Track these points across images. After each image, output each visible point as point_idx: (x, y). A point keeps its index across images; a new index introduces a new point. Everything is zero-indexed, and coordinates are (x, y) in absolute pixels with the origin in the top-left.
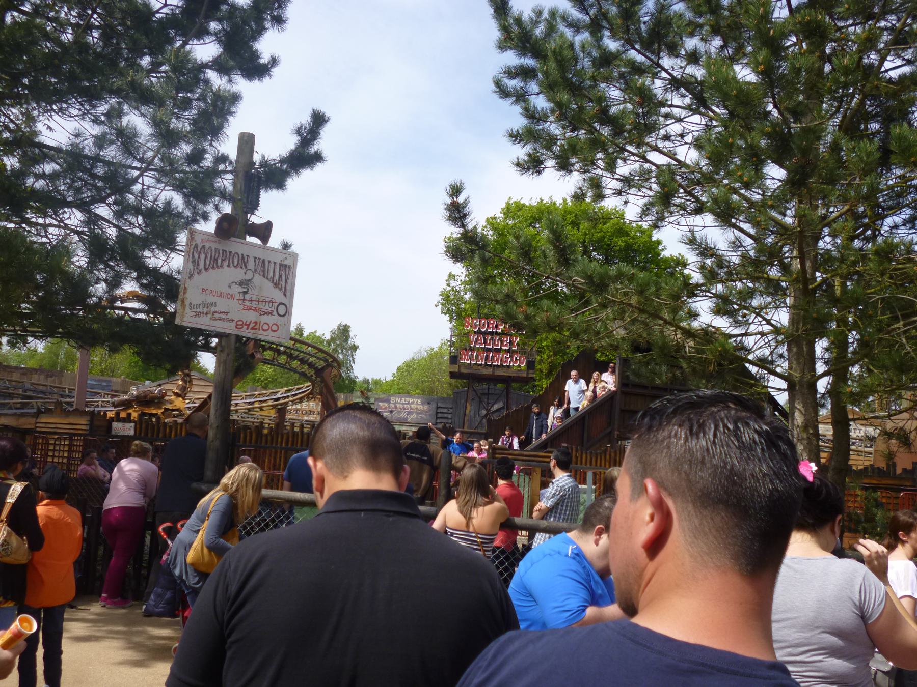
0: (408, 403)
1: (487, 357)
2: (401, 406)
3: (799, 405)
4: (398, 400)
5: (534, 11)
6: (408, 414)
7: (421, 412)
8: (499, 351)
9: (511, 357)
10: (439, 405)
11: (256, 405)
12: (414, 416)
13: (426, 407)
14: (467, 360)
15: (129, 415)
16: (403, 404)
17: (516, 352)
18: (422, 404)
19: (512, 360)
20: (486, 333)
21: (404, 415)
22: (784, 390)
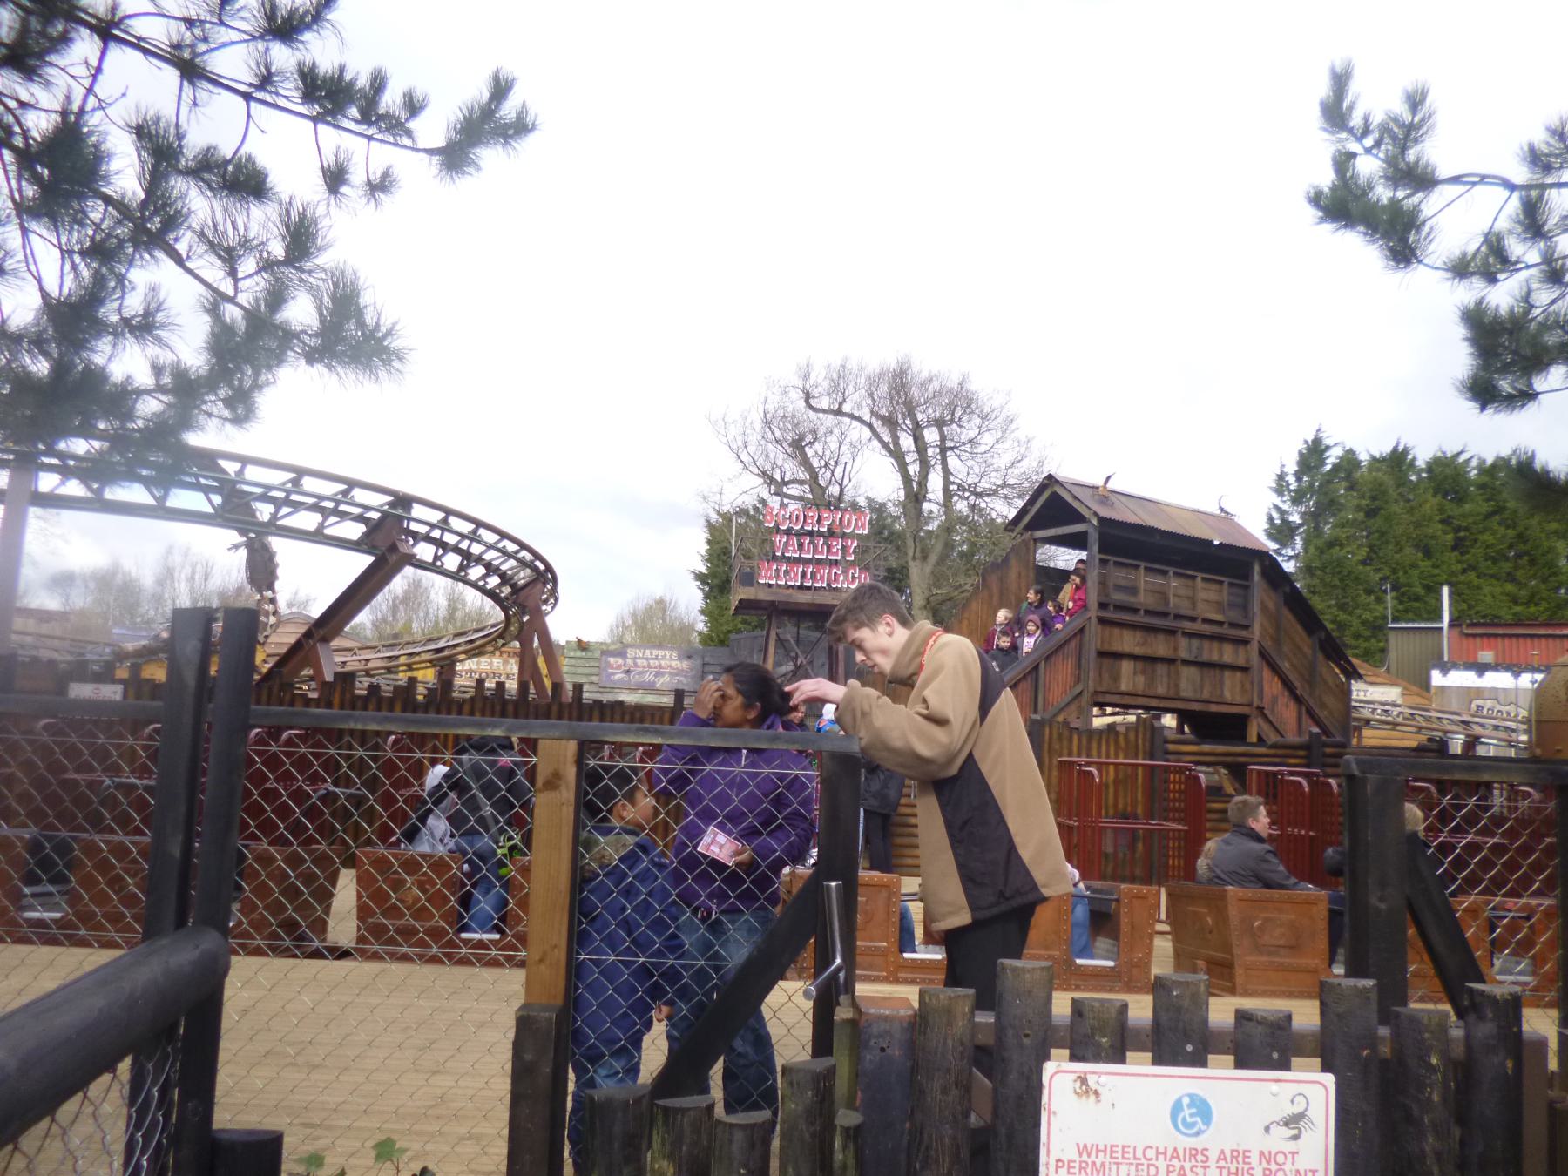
0: (656, 658)
1: (804, 575)
2: (645, 663)
4: (639, 653)
6: (656, 676)
7: (679, 672)
9: (845, 572)
10: (707, 659)
11: (402, 660)
12: (666, 678)
13: (685, 665)
14: (771, 578)
16: (647, 659)
17: (852, 564)
18: (680, 659)
21: (648, 677)
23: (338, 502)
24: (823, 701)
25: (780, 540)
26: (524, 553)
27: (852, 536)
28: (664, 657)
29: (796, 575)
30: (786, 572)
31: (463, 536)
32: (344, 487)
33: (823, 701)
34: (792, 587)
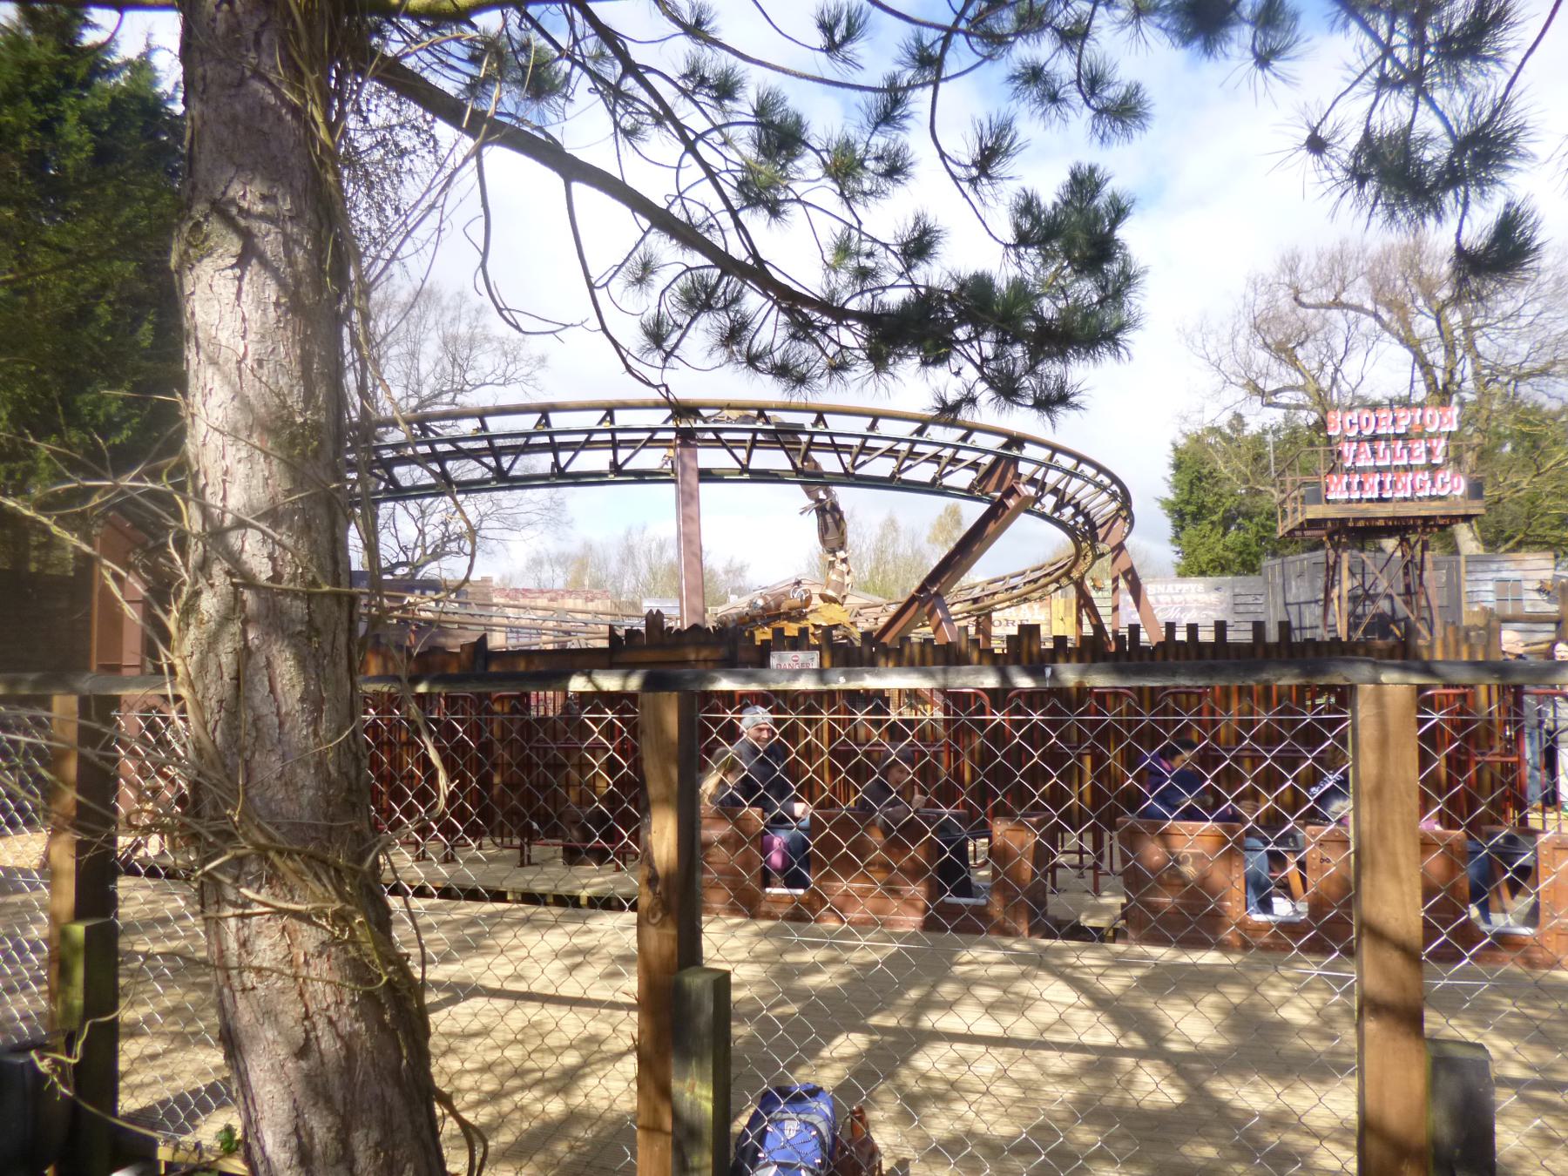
0: (1180, 592)
1: (1381, 483)
3: (875, 1020)
5: (1134, 92)
8: (1408, 468)
10: (1237, 590)
15: (1074, 516)
18: (1207, 591)
19: (1433, 485)
20: (1375, 438)
22: (629, 1007)
23: (914, 443)
24: (966, 628)
25: (1348, 450)
26: (1101, 477)
27: (1437, 435)
28: (1189, 591)
29: (1372, 486)
30: (1361, 484)
31: (1040, 464)
32: (918, 425)
33: (966, 628)
34: (1370, 500)
